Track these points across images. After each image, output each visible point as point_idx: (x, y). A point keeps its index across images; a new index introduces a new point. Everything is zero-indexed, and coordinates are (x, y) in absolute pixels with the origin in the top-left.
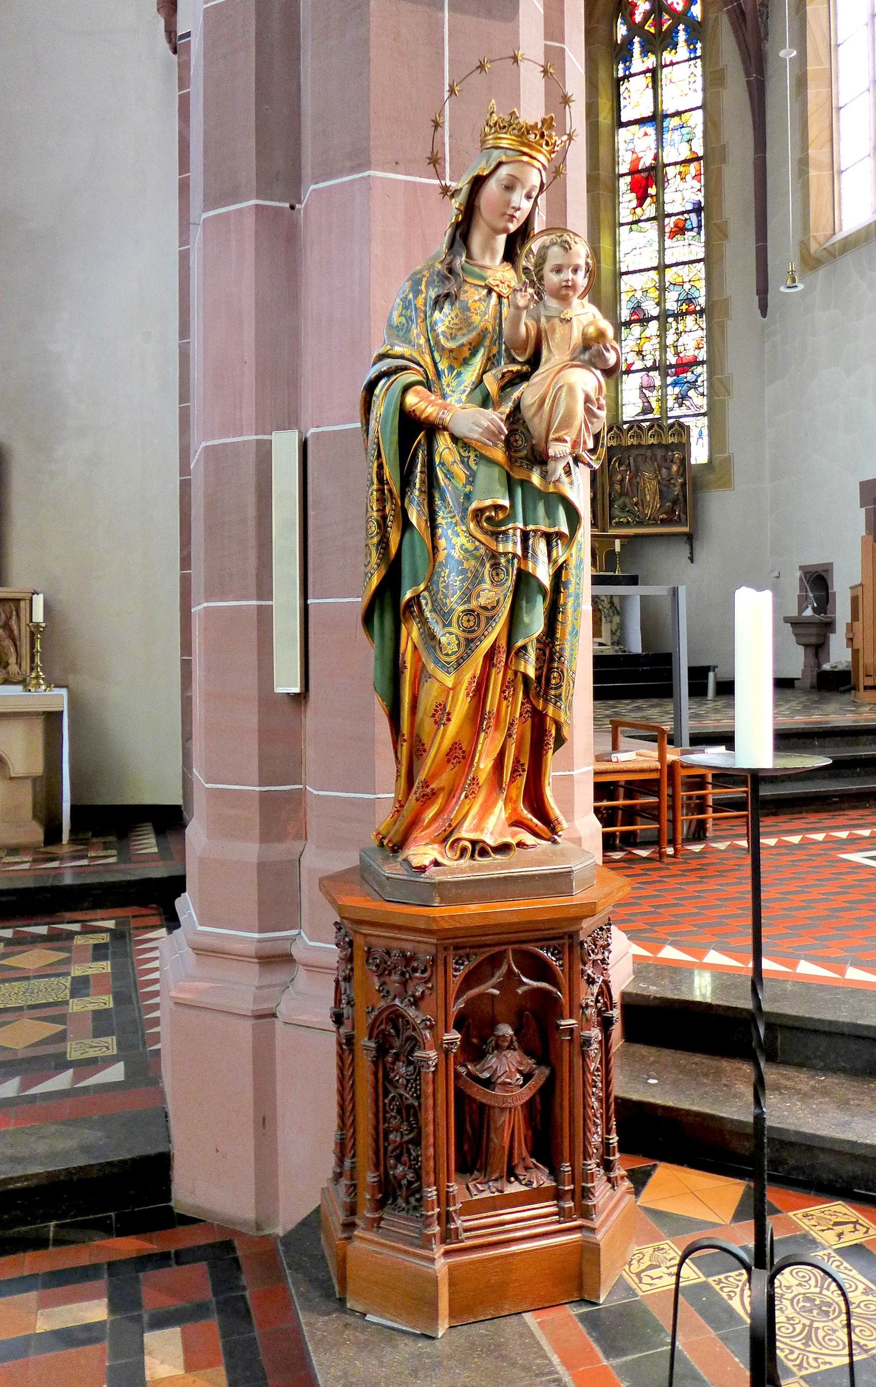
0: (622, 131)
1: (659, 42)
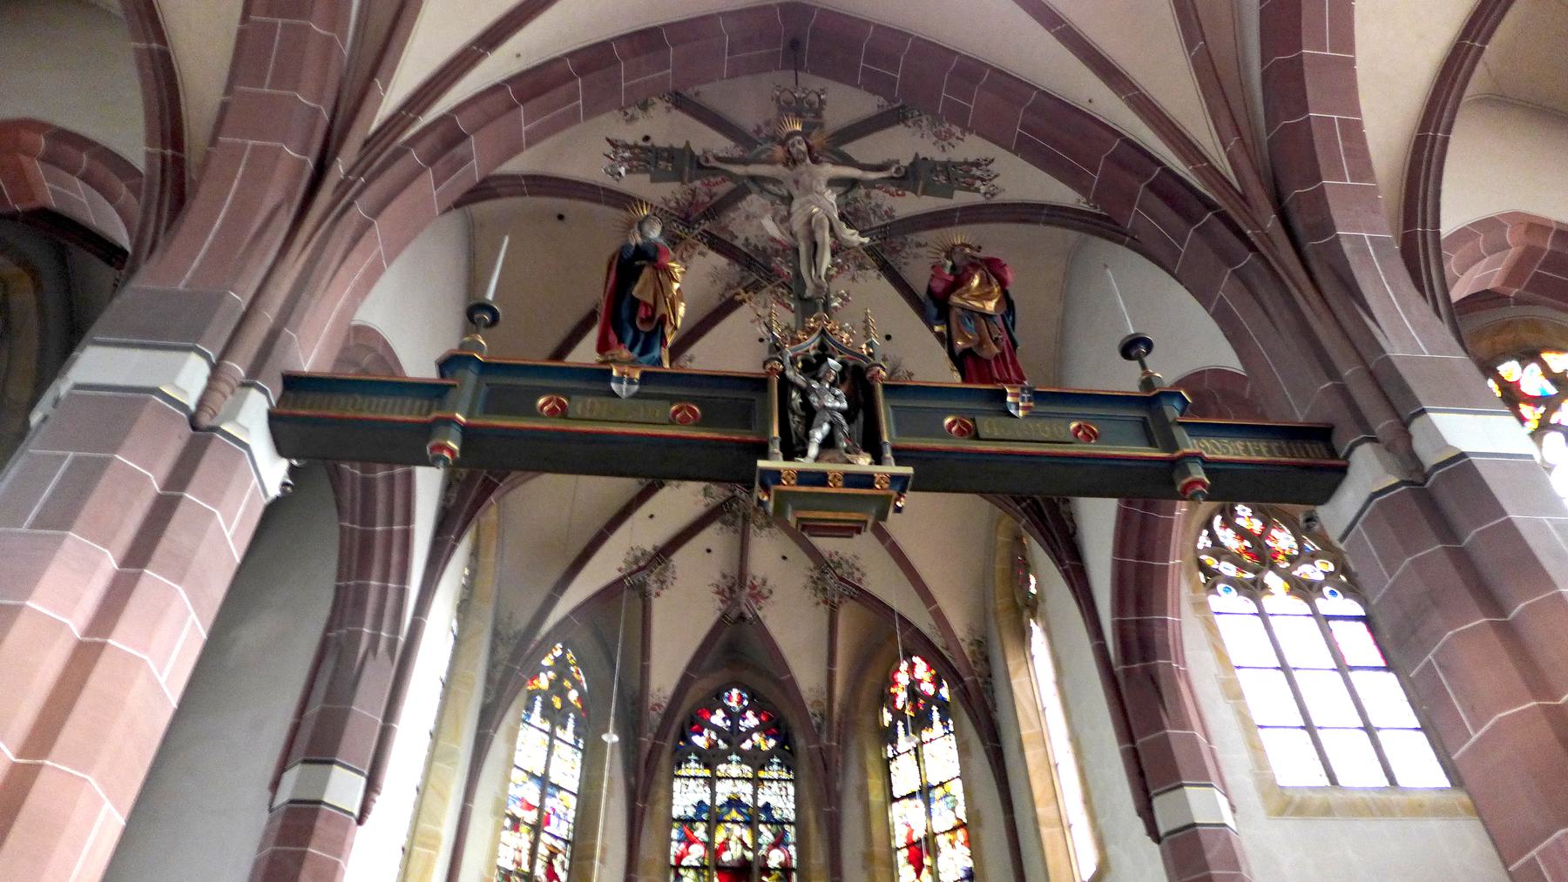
0: (895, 805)
1: (921, 722)
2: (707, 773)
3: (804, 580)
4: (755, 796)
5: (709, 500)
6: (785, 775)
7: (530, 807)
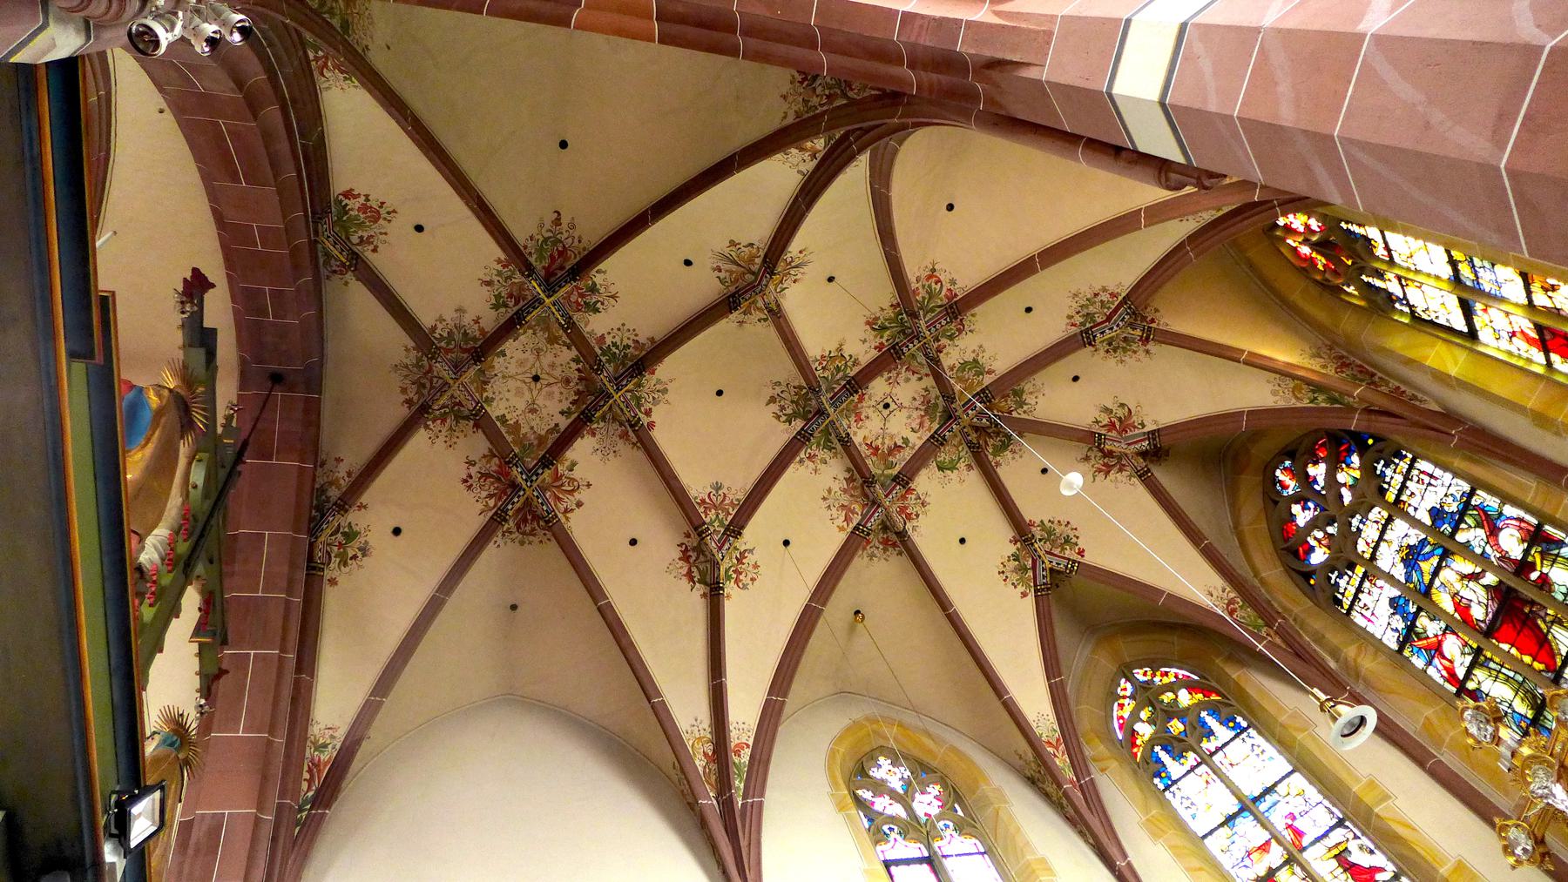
2: (1360, 570)
3: (1112, 362)
4: (1415, 523)
5: (962, 465)
6: (1403, 466)
7: (1264, 848)
